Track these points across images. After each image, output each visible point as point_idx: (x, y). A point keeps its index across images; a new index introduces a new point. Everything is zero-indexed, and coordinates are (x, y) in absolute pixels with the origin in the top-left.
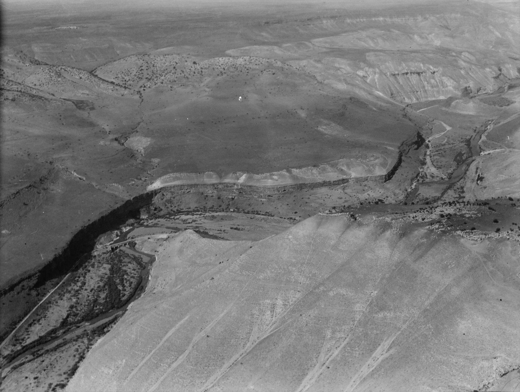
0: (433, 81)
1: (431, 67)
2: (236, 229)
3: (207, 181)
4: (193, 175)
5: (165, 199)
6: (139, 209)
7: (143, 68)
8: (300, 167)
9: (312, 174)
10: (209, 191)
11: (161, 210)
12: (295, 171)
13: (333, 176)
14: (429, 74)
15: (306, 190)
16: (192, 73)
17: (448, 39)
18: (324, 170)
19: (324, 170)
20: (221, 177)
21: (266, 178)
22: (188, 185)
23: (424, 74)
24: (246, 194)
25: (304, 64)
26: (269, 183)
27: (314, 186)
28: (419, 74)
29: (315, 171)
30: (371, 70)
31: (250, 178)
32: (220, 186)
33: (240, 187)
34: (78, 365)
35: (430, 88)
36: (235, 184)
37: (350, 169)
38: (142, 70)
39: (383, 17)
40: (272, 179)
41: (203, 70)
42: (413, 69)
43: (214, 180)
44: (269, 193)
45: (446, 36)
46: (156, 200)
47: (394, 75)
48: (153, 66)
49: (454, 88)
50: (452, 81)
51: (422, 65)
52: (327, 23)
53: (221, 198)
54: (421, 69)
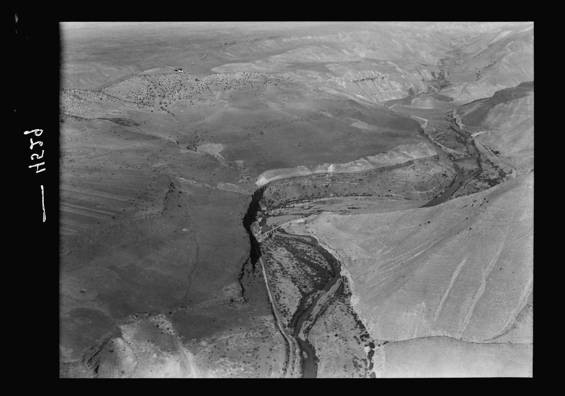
0: (384, 85)
1: (380, 74)
2: (353, 208)
3: (301, 173)
4: (288, 170)
5: (272, 193)
6: (257, 202)
7: (151, 87)
8: (373, 155)
9: (385, 159)
10: (305, 182)
11: (273, 202)
12: (371, 158)
13: (401, 160)
14: (380, 80)
15: (386, 172)
16: (201, 88)
17: (370, 51)
18: (392, 155)
19: (392, 155)
20: (311, 169)
21: (351, 165)
22: (288, 179)
23: (376, 80)
24: (338, 181)
25: (288, 76)
26: (357, 169)
27: (391, 168)
28: (372, 79)
29: (386, 157)
30: (338, 78)
31: (337, 167)
32: (314, 177)
33: (332, 175)
34: (358, 319)
35: (383, 91)
36: (326, 173)
37: (409, 153)
38: (151, 89)
39: (311, 35)
40: (357, 166)
41: (209, 86)
42: (367, 76)
43: (308, 173)
44: (359, 177)
45: (368, 49)
46: (266, 193)
47: (355, 82)
48: (160, 85)
49: (402, 89)
50: (399, 84)
51: (373, 72)
52: (269, 43)
53: (317, 186)
54: (373, 76)
